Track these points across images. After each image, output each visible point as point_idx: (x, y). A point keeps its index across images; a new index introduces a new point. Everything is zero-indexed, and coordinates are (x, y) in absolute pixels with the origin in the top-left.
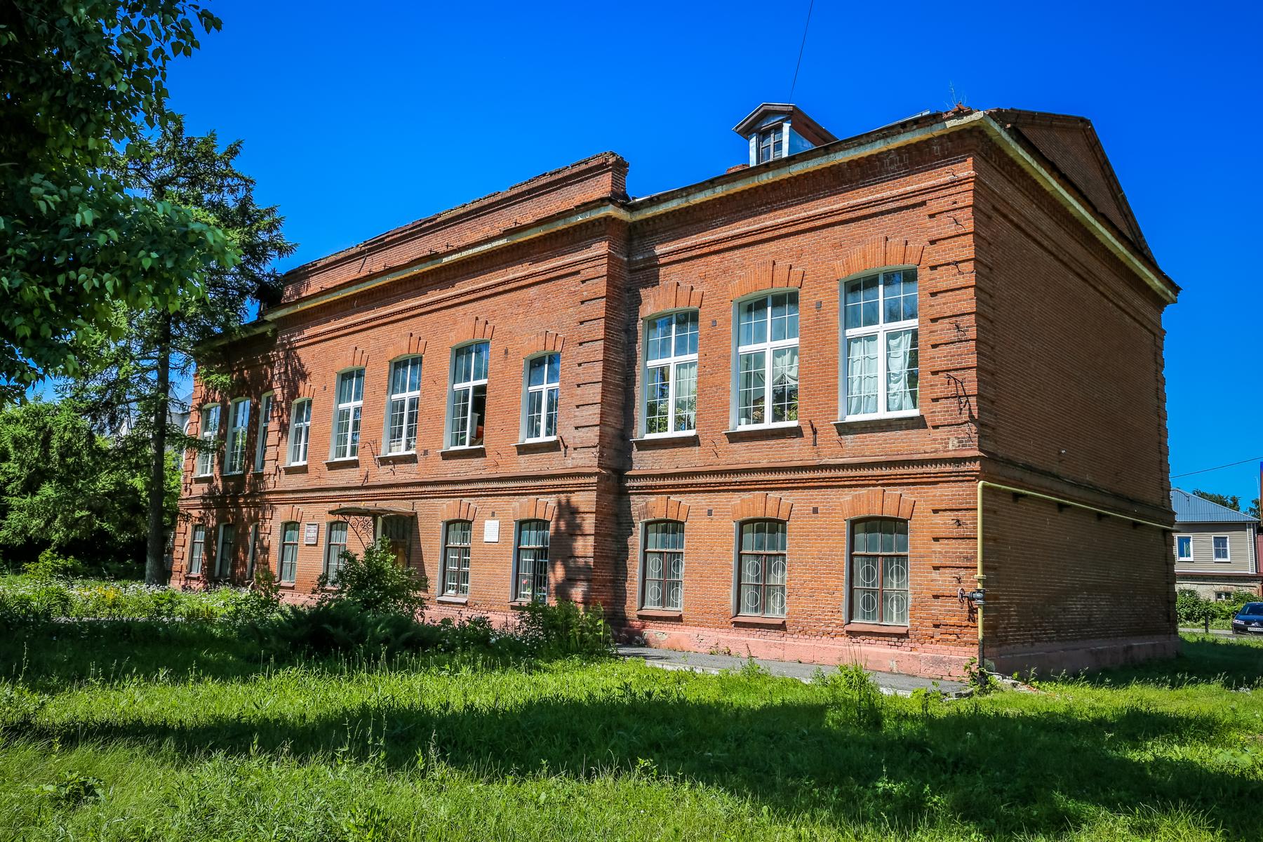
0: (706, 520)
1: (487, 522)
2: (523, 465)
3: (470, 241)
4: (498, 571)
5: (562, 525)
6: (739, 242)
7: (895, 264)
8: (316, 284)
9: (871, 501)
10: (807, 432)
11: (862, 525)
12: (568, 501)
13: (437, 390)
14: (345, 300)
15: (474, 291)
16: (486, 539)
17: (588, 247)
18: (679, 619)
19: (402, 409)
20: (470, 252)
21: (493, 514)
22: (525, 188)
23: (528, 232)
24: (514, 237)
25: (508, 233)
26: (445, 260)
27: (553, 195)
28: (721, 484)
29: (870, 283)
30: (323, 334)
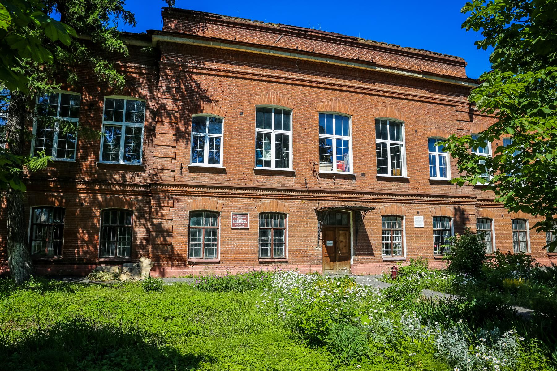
0: (501, 218)
1: (415, 217)
4: (425, 242)
5: (458, 218)
8: (212, 31)
9: (268, 205)
14: (237, 53)
15: (392, 93)
16: (416, 226)
20: (398, 72)
21: (418, 213)
22: (416, 52)
23: (435, 77)
24: (427, 76)
25: (424, 73)
26: (378, 69)
27: (435, 64)
28: (485, 205)
30: (235, 72)
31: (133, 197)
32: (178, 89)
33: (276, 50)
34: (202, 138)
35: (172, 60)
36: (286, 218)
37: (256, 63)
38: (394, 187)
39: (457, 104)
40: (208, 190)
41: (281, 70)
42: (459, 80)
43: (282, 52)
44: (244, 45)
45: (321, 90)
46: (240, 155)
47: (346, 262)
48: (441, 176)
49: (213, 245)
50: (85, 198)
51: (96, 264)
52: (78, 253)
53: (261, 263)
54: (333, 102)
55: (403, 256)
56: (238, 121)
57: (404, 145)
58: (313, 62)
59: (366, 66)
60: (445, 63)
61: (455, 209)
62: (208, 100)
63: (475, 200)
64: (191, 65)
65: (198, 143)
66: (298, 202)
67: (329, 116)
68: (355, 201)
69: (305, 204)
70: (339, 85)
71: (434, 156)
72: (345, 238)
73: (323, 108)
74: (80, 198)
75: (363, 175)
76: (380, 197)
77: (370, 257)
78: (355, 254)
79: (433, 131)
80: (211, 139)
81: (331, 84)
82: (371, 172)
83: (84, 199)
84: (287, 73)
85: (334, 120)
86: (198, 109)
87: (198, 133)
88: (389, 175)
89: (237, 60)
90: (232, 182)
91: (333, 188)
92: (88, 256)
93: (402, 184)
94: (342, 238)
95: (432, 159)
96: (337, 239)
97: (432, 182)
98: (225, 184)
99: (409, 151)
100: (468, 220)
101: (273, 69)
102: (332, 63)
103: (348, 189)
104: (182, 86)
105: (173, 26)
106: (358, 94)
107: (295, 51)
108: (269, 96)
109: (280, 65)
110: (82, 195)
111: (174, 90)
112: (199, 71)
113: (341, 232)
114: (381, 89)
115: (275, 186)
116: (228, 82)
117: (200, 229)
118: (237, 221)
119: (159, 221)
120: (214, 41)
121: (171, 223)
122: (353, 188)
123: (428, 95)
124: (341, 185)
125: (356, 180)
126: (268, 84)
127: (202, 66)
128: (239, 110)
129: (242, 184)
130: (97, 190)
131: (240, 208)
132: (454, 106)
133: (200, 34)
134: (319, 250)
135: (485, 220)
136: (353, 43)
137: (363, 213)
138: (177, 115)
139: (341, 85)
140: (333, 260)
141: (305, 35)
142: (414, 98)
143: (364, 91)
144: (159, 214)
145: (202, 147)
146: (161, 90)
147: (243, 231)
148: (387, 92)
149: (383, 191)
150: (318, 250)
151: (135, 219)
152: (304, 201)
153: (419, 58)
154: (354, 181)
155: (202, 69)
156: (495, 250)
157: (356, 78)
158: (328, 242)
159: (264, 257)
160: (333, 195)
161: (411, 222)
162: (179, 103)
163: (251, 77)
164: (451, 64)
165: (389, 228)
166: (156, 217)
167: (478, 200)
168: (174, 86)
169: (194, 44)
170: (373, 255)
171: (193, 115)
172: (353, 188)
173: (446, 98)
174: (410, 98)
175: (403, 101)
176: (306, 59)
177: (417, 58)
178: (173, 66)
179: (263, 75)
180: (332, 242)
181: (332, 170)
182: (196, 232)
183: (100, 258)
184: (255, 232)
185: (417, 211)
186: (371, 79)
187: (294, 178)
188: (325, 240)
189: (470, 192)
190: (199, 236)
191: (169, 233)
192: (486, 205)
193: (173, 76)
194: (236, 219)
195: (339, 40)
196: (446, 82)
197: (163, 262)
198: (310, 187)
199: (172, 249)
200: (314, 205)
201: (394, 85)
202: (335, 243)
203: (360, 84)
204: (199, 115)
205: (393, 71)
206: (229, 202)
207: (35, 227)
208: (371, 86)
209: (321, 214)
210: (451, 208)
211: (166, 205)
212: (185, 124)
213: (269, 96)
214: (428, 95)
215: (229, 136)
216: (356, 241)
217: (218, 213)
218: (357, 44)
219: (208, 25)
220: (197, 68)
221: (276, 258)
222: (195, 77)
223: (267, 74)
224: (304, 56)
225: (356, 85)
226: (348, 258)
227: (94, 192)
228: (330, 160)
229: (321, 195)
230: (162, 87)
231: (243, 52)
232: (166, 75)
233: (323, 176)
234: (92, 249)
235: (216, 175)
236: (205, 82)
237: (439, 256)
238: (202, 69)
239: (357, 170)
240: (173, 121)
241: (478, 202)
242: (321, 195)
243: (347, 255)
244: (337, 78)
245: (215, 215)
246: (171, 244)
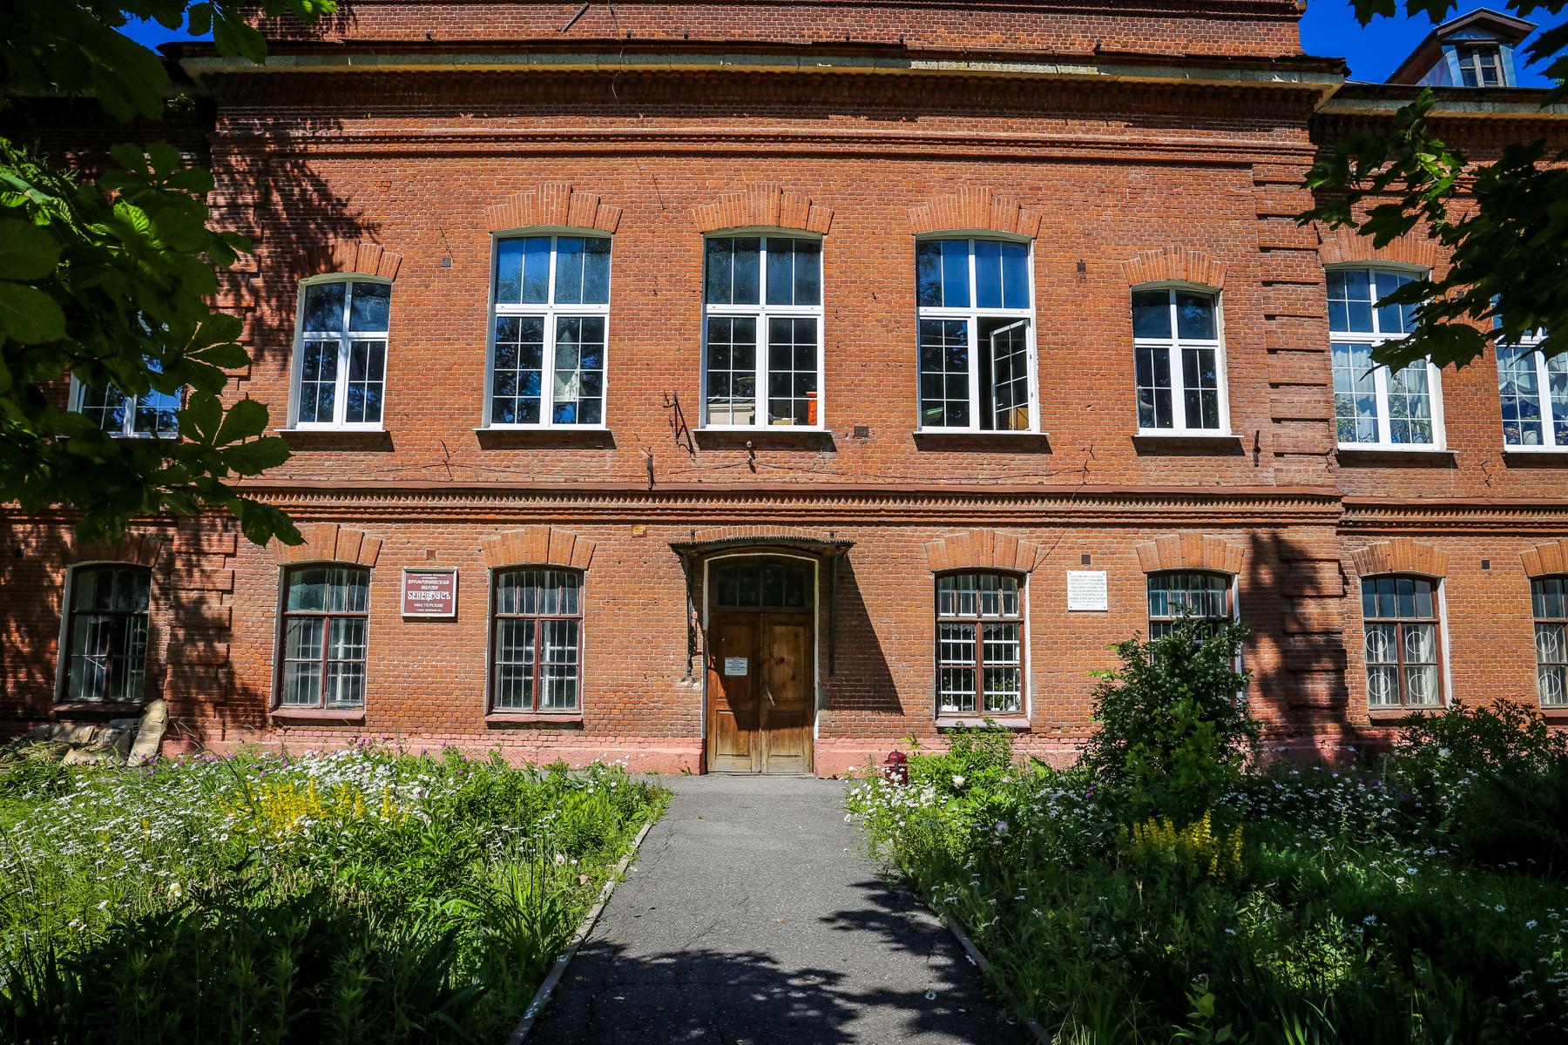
0: (1480, 576)
1: (1072, 575)
2: (1154, 475)
3: (938, 45)
6: (649, 146)
7: (580, 223)
9: (520, 544)
10: (1248, 448)
11: (510, 577)
12: (1275, 538)
13: (862, 319)
14: (599, 80)
15: (981, 142)
16: (1072, 605)
17: (1269, 129)
18: (578, 726)
19: (538, 335)
23: (1154, 70)
24: (1119, 69)
25: (1100, 57)
26: (917, 65)
29: (536, 243)
31: (152, 530)
32: (263, 206)
33: (548, 52)
34: (332, 348)
35: (251, 127)
36: (1021, 584)
37: (497, 101)
38: (986, 471)
39: (1257, 158)
40: (334, 502)
41: (577, 113)
42: (1260, 69)
43: (570, 56)
44: (449, 51)
45: (713, 161)
46: (438, 389)
47: (797, 731)
48: (1192, 422)
49: (528, 671)
50: (28, 535)
51: (48, 720)
53: (492, 725)
54: (750, 197)
55: (1021, 712)
56: (435, 285)
57: (1033, 322)
58: (654, 74)
59: (871, 60)
60: (1209, 17)
61: (1255, 540)
62: (352, 229)
63: (1337, 507)
64: (299, 133)
65: (319, 361)
66: (622, 532)
67: (956, 245)
68: (831, 524)
69: (645, 535)
70: (776, 138)
71: (1163, 354)
72: (796, 651)
73: (716, 217)
74: (14, 535)
76: (925, 505)
77: (883, 716)
78: (828, 706)
79: (1153, 263)
80: (358, 350)
81: (748, 138)
82: (894, 419)
83: (25, 541)
84: (598, 119)
85: (972, 258)
86: (319, 257)
87: (324, 334)
88: (974, 427)
89: (439, 100)
90: (410, 474)
91: (748, 481)
92: (28, 698)
93: (1018, 459)
94: (781, 650)
95: (1152, 367)
96: (765, 654)
98: (389, 482)
99: (1050, 338)
100: (1313, 582)
101: (551, 114)
102: (747, 68)
103: (804, 481)
104: (276, 197)
105: (255, 25)
106: (851, 162)
107: (632, 46)
108: (534, 199)
109: (574, 99)
110: (19, 528)
111: (251, 211)
112: (323, 148)
113: (778, 629)
114: (939, 134)
115: (544, 481)
116: (410, 171)
117: (319, 618)
118: (420, 595)
119: (195, 595)
120: (357, 52)
121: (228, 601)
122: (823, 478)
124: (776, 470)
125: (834, 450)
126: (535, 161)
127: (334, 132)
128: (440, 253)
129: (441, 479)
130: (56, 511)
131: (431, 554)
132: (1248, 165)
133: (332, 37)
134: (690, 689)
138: (258, 282)
139: (784, 138)
140: (749, 720)
142: (1074, 153)
143: (874, 149)
144: (197, 574)
145: (331, 373)
146: (216, 214)
147: (440, 625)
148: (962, 141)
149: (943, 485)
150: (689, 690)
151: (157, 592)
152: (643, 527)
153: (1098, 13)
154: (828, 454)
155: (329, 140)
156: (1449, 703)
157: (842, 108)
158: (728, 662)
159: (512, 709)
160: (430, 503)
162: (263, 251)
163: (477, 147)
164: (1234, 18)
165: (972, 616)
166: (186, 585)
167: (1349, 507)
168: (249, 199)
169: (301, 69)
170: (899, 710)
171: (303, 283)
172: (821, 480)
173: (1210, 140)
174: (1057, 152)
175: (1028, 166)
176: (654, 67)
177: (1090, 13)
178: (249, 143)
179: (515, 138)
180: (744, 662)
181: (752, 420)
182: (307, 629)
183: (60, 702)
184: (477, 623)
185: (1079, 553)
186: (899, 104)
187: (609, 452)
188: (717, 650)
189: (1312, 478)
191: (222, 629)
192: (1406, 524)
193: (250, 172)
194: (417, 588)
196: (1203, 82)
197: (203, 714)
198: (663, 482)
199: (231, 674)
201: (992, 115)
202: (755, 666)
203: (860, 126)
204: (322, 278)
205: (945, 65)
206: (397, 534)
207: (500, 623)
208: (901, 129)
210: (1236, 541)
211: (215, 549)
212: (279, 309)
213: (534, 199)
215: (407, 334)
216: (831, 658)
217: (580, 572)
219: (355, 8)
220: (318, 141)
221: (565, 714)
222: (314, 166)
223: (531, 130)
224: (644, 57)
225: (471, 130)
226: (801, 719)
227: (49, 518)
228: (746, 389)
229: (700, 504)
230: (216, 206)
231: (450, 73)
232: (229, 170)
233: (710, 441)
234: (39, 678)
235: (361, 456)
236: (340, 177)
238: (329, 140)
239: (839, 418)
240: (244, 304)
242: (700, 504)
243: (798, 707)
244: (771, 114)
245: (358, 575)
246: (226, 663)
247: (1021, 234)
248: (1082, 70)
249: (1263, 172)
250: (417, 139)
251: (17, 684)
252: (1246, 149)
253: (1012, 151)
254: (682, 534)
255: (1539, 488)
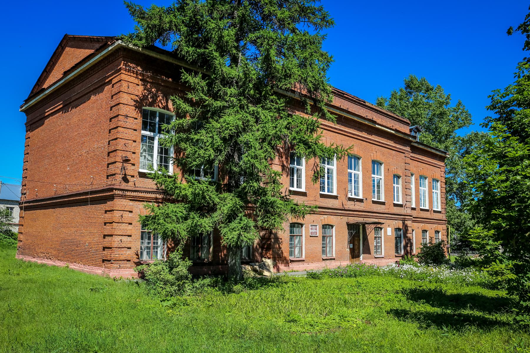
6: (344, 133)
15: (380, 142)
25: (396, 130)
26: (377, 126)
52: (221, 256)
75: (366, 199)
76: (374, 214)
78: (363, 253)
81: (354, 134)
97: (322, 196)
122: (362, 208)
123: (394, 145)
135: (296, 225)
136: (362, 104)
137: (366, 225)
141: (343, 96)
161: (386, 232)
172: (362, 208)
190: (157, 240)
195: (358, 102)
198: (346, 207)
200: (345, 219)
205: (383, 128)
209: (350, 226)
214: (394, 145)
218: (365, 106)
226: (359, 256)
237: (397, 255)
241: (414, 219)
247: (382, 161)
248: (392, 131)
249: (406, 155)
250: (437, 164)
251: (224, 254)
252: (405, 150)
253: (383, 145)
254: (353, 220)
255: (437, 217)
